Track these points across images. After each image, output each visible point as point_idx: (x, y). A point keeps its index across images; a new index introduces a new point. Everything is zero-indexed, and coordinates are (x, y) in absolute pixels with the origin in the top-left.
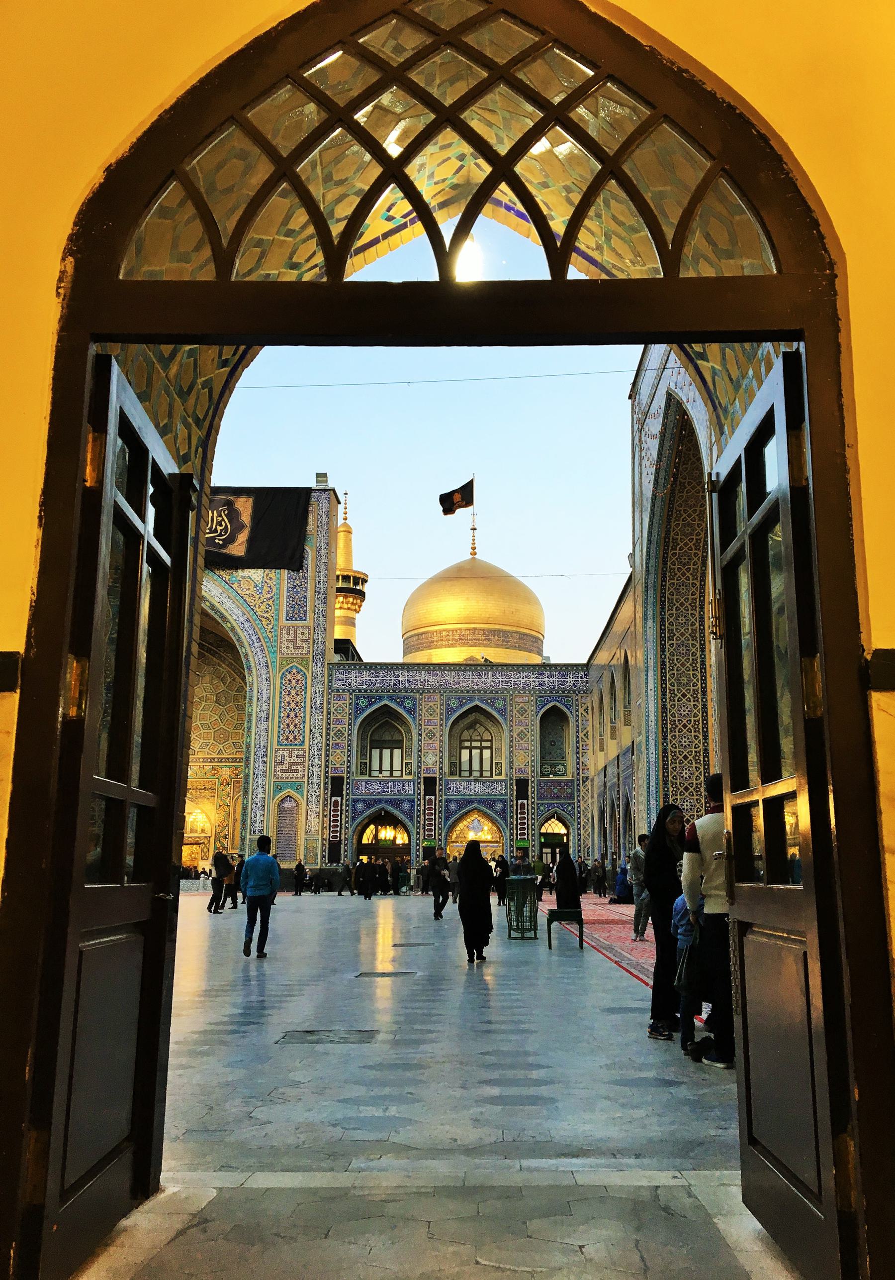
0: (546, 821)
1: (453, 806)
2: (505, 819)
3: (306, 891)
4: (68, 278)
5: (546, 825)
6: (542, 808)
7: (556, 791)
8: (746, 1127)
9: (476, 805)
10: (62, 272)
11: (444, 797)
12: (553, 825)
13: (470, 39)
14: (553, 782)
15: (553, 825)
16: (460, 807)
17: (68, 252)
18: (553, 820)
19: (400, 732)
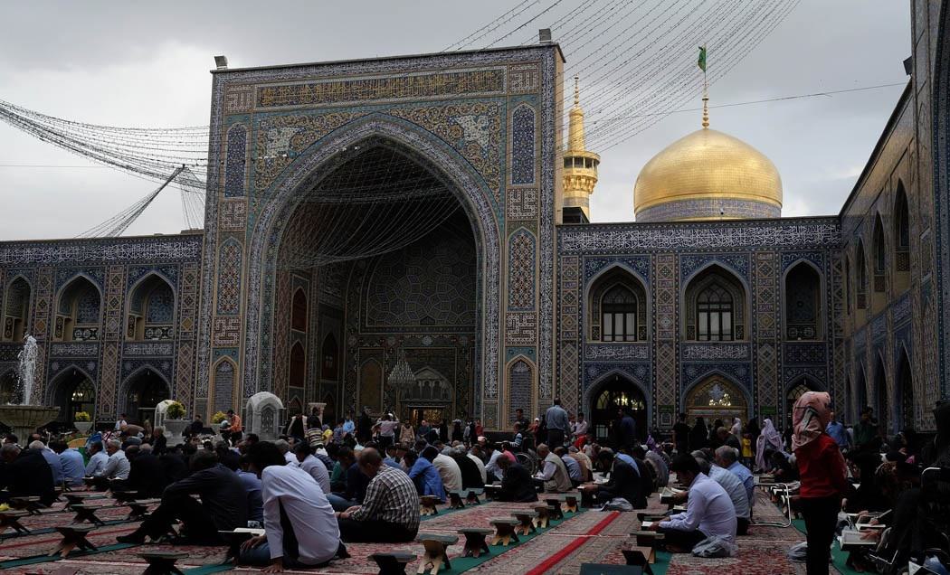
1: (691, 371)
16: (699, 372)
19: (635, 298)
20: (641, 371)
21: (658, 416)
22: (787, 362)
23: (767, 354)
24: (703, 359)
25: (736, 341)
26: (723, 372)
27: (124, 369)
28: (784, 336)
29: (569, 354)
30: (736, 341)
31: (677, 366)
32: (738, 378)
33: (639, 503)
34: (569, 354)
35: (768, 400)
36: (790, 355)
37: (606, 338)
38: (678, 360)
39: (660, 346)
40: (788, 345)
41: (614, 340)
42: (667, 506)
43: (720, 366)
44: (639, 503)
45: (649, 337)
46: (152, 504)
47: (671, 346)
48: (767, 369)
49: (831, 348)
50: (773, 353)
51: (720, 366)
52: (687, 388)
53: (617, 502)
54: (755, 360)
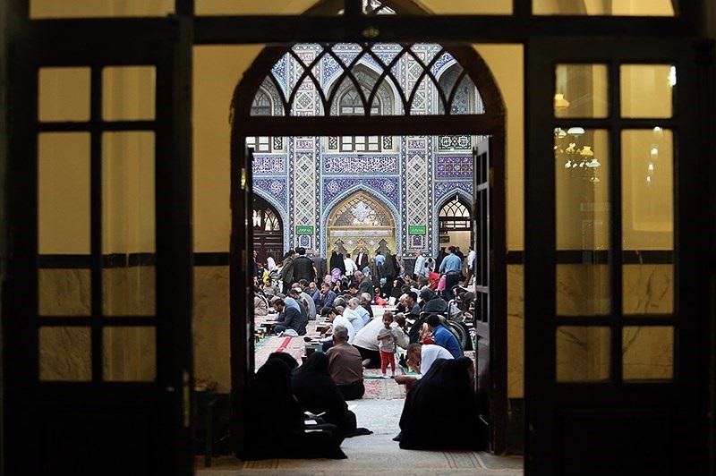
0: (446, 203)
1: (333, 187)
2: (396, 202)
3: (400, 435)
4: (233, 116)
5: (446, 207)
6: (440, 188)
7: (457, 168)
8: (88, 293)
9: (361, 185)
10: (231, 114)
11: (322, 176)
12: (454, 208)
13: (426, 76)
14: (454, 157)
15: (454, 208)
16: (342, 188)
17: (232, 106)
18: (454, 202)
19: (269, 99)
20: (276, 187)
21: (296, 239)
22: (438, 176)
23: (417, 167)
24: (347, 173)
25: (384, 152)
26: (367, 188)
27: (326, 192)
28: (435, 148)
29: (305, 168)
30: (384, 152)
31: (317, 181)
32: (385, 194)
33: (302, 331)
34: (305, 168)
35: (305, 220)
36: (441, 168)
37: (344, 148)
38: (318, 175)
39: (298, 157)
40: (438, 157)
41: (354, 148)
42: (320, 333)
43: (366, 181)
44: (302, 331)
45: (286, 148)
46: (390, 365)
47: (311, 157)
48: (417, 184)
49: (404, 160)
50: (424, 166)
51: (366, 181)
52: (329, 207)
53: (288, 332)
54: (404, 173)
